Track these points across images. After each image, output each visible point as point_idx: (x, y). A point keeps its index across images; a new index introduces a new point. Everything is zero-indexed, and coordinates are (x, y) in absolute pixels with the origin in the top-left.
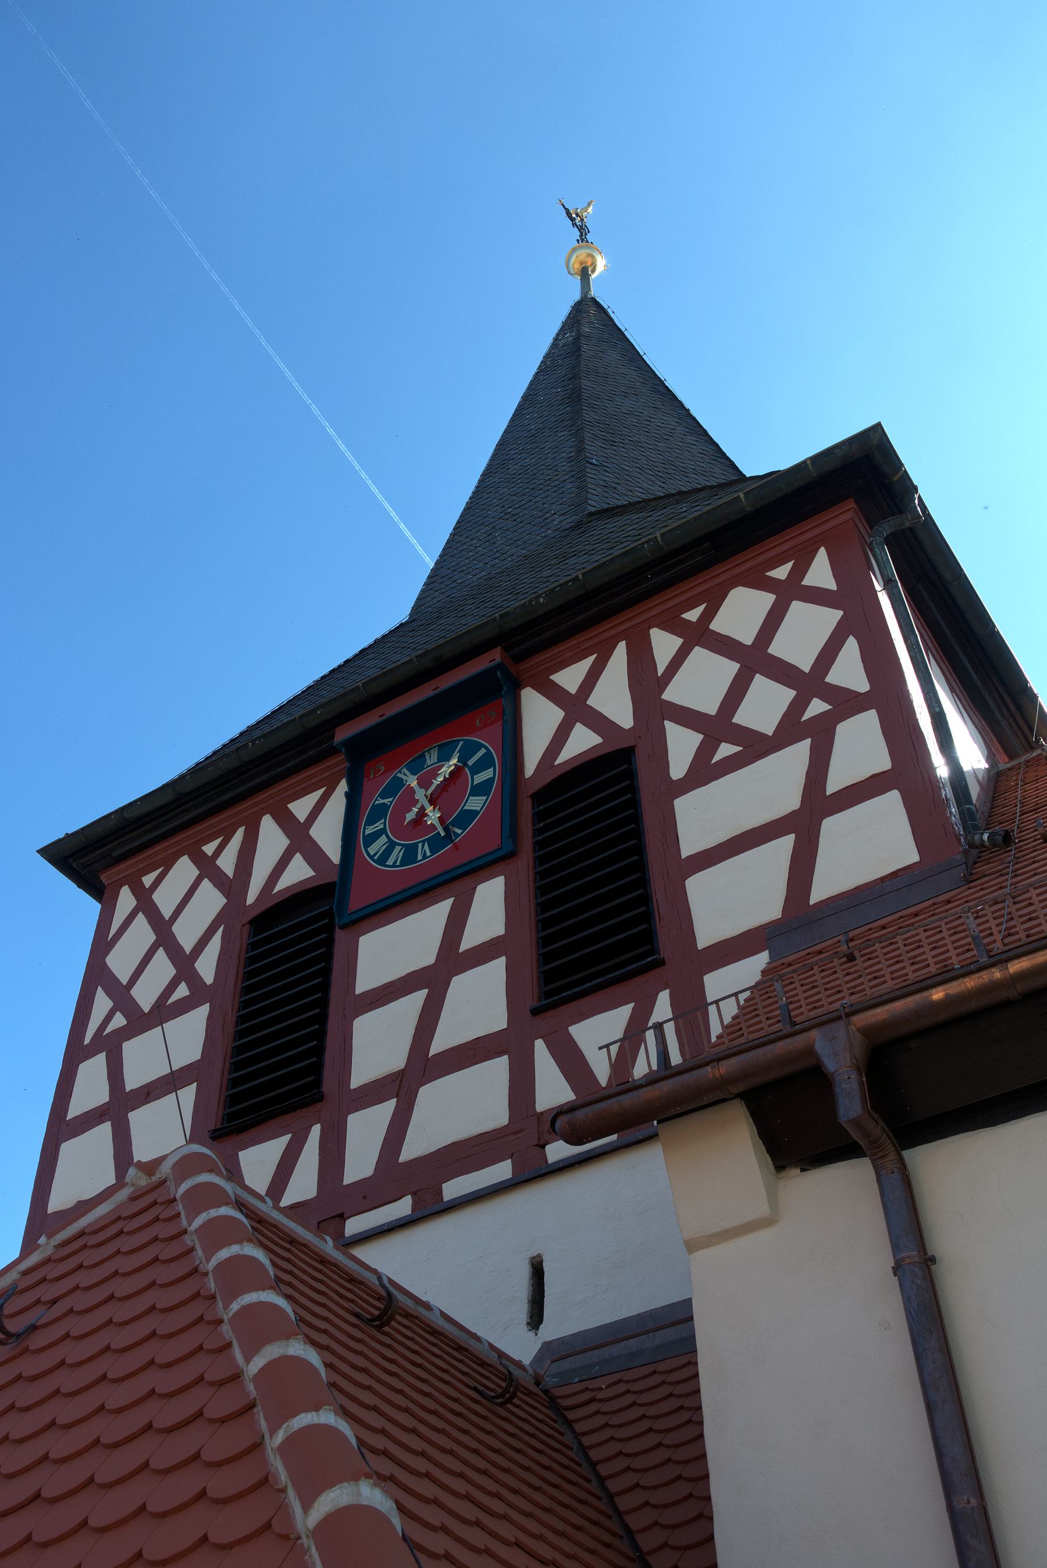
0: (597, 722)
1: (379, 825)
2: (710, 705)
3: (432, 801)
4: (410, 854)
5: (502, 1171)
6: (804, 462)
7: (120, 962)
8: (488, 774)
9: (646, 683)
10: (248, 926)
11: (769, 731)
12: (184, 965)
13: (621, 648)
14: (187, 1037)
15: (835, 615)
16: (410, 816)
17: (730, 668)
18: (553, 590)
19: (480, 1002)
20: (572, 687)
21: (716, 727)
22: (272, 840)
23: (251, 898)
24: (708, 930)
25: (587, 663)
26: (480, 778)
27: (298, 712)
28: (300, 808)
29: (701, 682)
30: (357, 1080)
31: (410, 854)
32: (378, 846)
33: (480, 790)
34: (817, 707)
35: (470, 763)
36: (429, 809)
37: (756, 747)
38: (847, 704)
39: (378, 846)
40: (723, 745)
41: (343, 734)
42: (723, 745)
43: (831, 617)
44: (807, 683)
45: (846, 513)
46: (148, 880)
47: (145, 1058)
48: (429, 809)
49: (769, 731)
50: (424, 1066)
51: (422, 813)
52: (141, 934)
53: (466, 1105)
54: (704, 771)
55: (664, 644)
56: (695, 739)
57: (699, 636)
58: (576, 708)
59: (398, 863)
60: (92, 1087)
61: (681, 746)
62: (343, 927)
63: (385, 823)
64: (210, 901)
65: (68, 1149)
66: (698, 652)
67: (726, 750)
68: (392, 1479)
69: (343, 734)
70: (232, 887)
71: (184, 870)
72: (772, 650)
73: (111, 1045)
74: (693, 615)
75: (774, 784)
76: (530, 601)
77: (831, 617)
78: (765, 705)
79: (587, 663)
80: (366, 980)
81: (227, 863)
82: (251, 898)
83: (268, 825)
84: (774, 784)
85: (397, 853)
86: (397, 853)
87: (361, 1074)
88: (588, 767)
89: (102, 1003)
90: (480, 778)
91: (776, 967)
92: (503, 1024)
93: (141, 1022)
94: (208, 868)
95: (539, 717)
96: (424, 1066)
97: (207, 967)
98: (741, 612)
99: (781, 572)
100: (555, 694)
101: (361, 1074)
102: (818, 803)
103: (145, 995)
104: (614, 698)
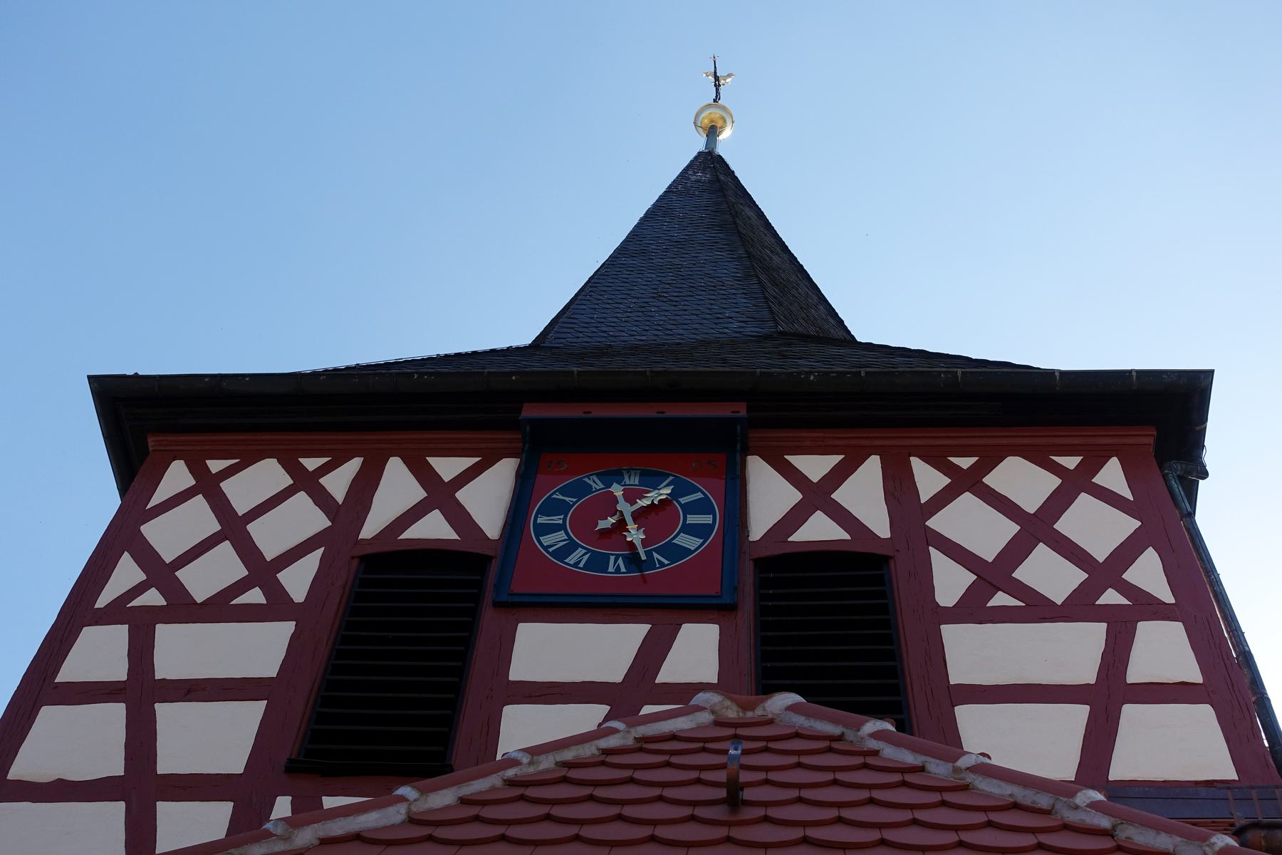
0: (458, 516)
3: (636, 516)
4: (598, 562)
6: (1130, 372)
10: (355, 563)
11: (200, 597)
14: (261, 648)
15: (1131, 525)
16: (604, 524)
17: (214, 526)
18: (827, 374)
21: (993, 575)
25: (468, 462)
29: (974, 526)
31: (598, 562)
34: (152, 598)
35: (683, 500)
36: (632, 526)
40: (1110, 591)
41: (531, 412)
42: (1110, 591)
44: (262, 571)
45: (1146, 438)
47: (181, 651)
48: (632, 526)
49: (200, 597)
51: (621, 524)
54: (972, 609)
56: (966, 578)
57: (208, 487)
59: (581, 565)
60: (100, 654)
62: (498, 605)
63: (564, 520)
64: (301, 519)
66: (199, 500)
67: (1001, 599)
69: (531, 412)
72: (249, 527)
74: (311, 464)
75: (1075, 651)
76: (800, 373)
79: (468, 462)
81: (338, 483)
83: (396, 469)
88: (430, 553)
89: (127, 573)
91: (1205, 825)
92: (239, 769)
93: (183, 609)
95: (397, 489)
97: (298, 581)
98: (256, 481)
99: (965, 463)
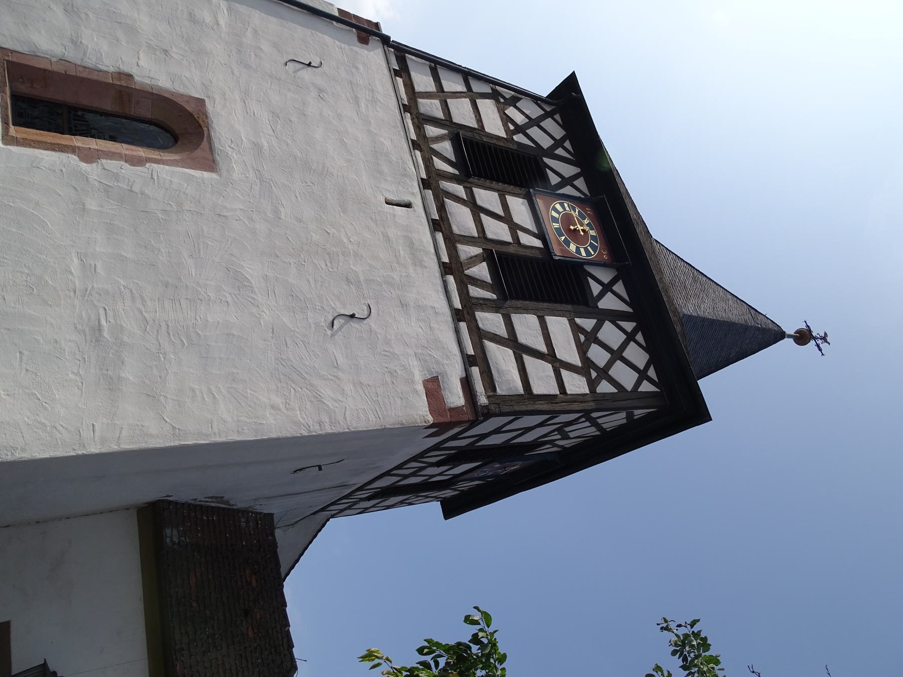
0: (601, 295)
1: (567, 209)
2: (601, 335)
5: (445, 259)
7: (524, 104)
8: (584, 254)
9: (614, 317)
12: (520, 129)
13: (630, 310)
14: (494, 126)
19: (497, 231)
20: (615, 288)
21: (592, 337)
22: (568, 170)
23: (546, 160)
24: (516, 318)
26: (582, 250)
27: (631, 212)
28: (567, 144)
30: (475, 190)
32: (558, 207)
33: (578, 250)
34: (594, 374)
37: (582, 350)
38: (592, 384)
39: (558, 207)
43: (629, 386)
46: (557, 117)
50: (477, 210)
52: (535, 112)
53: (462, 219)
54: (577, 329)
55: (629, 326)
57: (630, 337)
58: (607, 288)
61: (588, 324)
64: (546, 142)
65: (459, 78)
67: (582, 338)
68: (342, 511)
70: (550, 153)
71: (559, 133)
73: (494, 96)
75: (568, 352)
77: (629, 386)
78: (598, 356)
80: (510, 199)
81: (560, 151)
82: (546, 160)
84: (568, 352)
85: (554, 214)
86: (554, 214)
87: (477, 191)
90: (582, 250)
94: (558, 143)
96: (477, 210)
97: (519, 138)
98: (637, 355)
100: (613, 282)
101: (477, 191)
102: (558, 365)
103: (511, 112)
104: (609, 302)
